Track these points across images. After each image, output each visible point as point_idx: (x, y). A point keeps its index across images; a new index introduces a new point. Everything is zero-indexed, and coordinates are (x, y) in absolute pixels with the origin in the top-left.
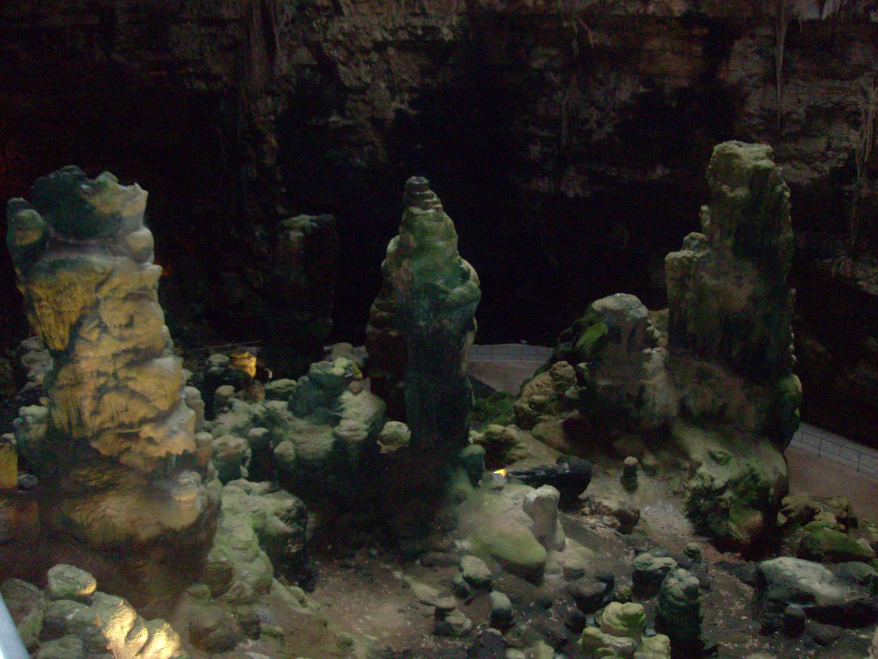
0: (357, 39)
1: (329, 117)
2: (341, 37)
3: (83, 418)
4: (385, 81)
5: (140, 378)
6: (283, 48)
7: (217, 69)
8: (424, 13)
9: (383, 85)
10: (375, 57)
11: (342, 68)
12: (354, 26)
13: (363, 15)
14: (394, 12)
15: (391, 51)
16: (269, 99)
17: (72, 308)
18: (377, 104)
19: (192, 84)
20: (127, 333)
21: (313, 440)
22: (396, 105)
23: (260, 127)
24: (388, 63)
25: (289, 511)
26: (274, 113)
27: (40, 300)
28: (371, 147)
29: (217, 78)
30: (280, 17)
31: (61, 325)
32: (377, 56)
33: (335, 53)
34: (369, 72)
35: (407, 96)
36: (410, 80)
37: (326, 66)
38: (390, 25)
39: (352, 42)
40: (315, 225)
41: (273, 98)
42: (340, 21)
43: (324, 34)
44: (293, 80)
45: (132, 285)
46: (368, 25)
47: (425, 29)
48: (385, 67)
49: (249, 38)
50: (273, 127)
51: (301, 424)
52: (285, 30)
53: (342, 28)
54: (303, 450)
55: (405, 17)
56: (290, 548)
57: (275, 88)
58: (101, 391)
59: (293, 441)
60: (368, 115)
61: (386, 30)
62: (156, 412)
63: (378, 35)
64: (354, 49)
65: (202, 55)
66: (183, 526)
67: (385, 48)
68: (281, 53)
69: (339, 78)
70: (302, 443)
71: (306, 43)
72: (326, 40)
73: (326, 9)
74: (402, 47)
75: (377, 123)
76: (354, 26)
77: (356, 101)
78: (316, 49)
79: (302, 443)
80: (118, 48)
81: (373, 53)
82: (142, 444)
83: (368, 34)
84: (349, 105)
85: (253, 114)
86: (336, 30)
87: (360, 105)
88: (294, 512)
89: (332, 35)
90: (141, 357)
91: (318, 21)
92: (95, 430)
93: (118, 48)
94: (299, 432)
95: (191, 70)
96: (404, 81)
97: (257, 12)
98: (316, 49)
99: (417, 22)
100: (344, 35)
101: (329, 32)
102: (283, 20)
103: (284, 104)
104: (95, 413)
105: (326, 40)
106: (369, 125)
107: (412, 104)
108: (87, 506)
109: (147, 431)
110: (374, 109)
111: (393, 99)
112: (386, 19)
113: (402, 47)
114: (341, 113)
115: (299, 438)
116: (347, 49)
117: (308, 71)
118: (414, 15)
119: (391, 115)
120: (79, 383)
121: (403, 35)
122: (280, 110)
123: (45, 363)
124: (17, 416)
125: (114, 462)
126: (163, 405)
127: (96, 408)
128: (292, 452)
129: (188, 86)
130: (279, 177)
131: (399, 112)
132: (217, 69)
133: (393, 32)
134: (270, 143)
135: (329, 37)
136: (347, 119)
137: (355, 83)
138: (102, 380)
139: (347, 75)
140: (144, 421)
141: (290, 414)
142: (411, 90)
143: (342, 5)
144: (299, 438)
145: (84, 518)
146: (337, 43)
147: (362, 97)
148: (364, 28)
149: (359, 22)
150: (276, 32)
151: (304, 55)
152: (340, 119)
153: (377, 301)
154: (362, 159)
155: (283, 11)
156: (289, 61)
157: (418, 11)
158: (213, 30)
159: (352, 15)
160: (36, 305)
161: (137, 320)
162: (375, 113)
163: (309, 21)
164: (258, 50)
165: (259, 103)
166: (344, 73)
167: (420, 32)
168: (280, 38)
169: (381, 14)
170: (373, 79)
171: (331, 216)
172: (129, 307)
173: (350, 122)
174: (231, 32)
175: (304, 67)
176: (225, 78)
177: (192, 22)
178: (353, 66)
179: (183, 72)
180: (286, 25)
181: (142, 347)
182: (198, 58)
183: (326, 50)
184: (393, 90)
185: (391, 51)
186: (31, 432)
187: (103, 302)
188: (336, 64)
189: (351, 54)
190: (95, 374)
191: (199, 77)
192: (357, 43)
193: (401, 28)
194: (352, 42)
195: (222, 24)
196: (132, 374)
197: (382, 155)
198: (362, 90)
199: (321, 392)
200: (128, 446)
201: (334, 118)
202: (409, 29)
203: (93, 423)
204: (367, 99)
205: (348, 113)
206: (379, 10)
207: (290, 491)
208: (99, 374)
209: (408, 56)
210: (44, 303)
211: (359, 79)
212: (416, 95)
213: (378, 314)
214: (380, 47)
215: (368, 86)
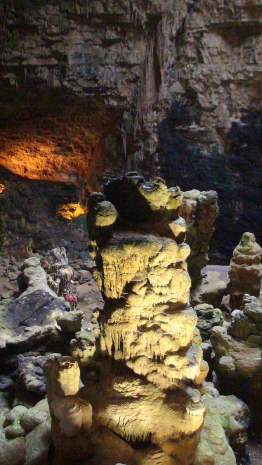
0: (212, 78)
1: (190, 125)
2: (201, 77)
3: (124, 346)
4: (226, 105)
5: (170, 323)
6: (165, 82)
7: (125, 93)
8: (255, 63)
9: (225, 107)
10: (221, 89)
11: (200, 96)
12: (210, 70)
13: (216, 63)
14: (236, 62)
15: (232, 86)
16: (155, 112)
17: (130, 273)
18: (221, 118)
19: (108, 102)
20: (164, 291)
21: (248, 358)
22: (232, 119)
23: (148, 129)
24: (229, 93)
25: (239, 412)
26: (157, 121)
27: (108, 264)
28: (214, 145)
29: (125, 98)
30: (165, 63)
31: (120, 283)
32: (223, 89)
33: (197, 86)
34: (217, 99)
35: (239, 114)
36: (243, 105)
37: (191, 94)
38: (232, 71)
39: (208, 80)
40: (205, 197)
41: (157, 113)
42: (201, 67)
43: (191, 74)
44: (170, 102)
45: (174, 260)
46: (219, 70)
47: (254, 72)
48: (228, 96)
49: (145, 75)
50: (156, 129)
51: (239, 345)
52: (168, 71)
53: (202, 71)
54: (241, 365)
55: (242, 66)
56: (240, 440)
57: (158, 106)
58: (143, 329)
59: (233, 357)
60: (214, 125)
61: (230, 73)
62: (179, 347)
63: (225, 76)
64: (209, 84)
65: (116, 84)
66: (191, 431)
67: (228, 84)
68: (164, 86)
69: (198, 102)
70: (240, 359)
71: (180, 80)
72: (192, 78)
73: (193, 59)
74: (239, 84)
75: (220, 130)
76: (210, 70)
77: (208, 116)
78: (185, 83)
79: (240, 359)
80: (67, 79)
81: (220, 87)
82: (166, 368)
83: (219, 76)
84: (203, 118)
85: (145, 121)
86: (198, 73)
87: (210, 119)
88: (243, 413)
89: (196, 75)
90: (175, 308)
91: (188, 66)
92: (132, 356)
93: (67, 79)
94: (237, 351)
95: (109, 93)
96: (239, 105)
97: (151, 60)
98: (185, 83)
99: (250, 68)
100: (204, 75)
101: (194, 73)
102: (166, 65)
103: (163, 116)
104: (134, 344)
105: (192, 78)
106: (214, 131)
107: (243, 119)
108: (125, 411)
109: (171, 360)
110: (219, 121)
111: (231, 116)
112: (230, 66)
113: (239, 84)
114: (198, 123)
115: (237, 355)
116: (205, 84)
117: (179, 97)
118: (249, 64)
119: (229, 126)
120: (127, 322)
121: (241, 77)
122: (160, 120)
123: (39, 275)
124: (74, 337)
125: (143, 380)
126: (184, 343)
127: (136, 340)
128: (232, 365)
129: (106, 103)
130: (157, 160)
131: (234, 124)
132: (124, 94)
133: (235, 74)
134: (153, 139)
135: (194, 77)
136: (201, 127)
137: (208, 105)
138: (144, 322)
139: (203, 100)
140: (170, 353)
141: (230, 337)
142: (243, 110)
143: (204, 57)
144: (237, 355)
145: (122, 419)
146: (199, 80)
147: (212, 114)
148: (216, 72)
149: (213, 67)
150: (162, 72)
151: (178, 87)
152: (197, 126)
153: (239, 247)
154: (208, 152)
155: (167, 60)
156: (168, 90)
157: (252, 62)
158: (124, 70)
159: (209, 63)
160: (105, 267)
161: (174, 283)
162: (219, 123)
163: (182, 66)
164: (150, 83)
165: (148, 115)
166: (202, 99)
167: (251, 75)
168: (164, 75)
169: (228, 63)
170: (219, 103)
171: (215, 192)
172: (171, 273)
173: (203, 129)
174: (134, 72)
175: (177, 94)
176: (128, 99)
177: (112, 65)
178: (208, 95)
179: (104, 94)
180: (169, 68)
181: (174, 301)
182: (114, 86)
183: (191, 84)
184: (232, 110)
185: (232, 86)
186: (85, 352)
187: (153, 269)
188: (196, 93)
189: (207, 87)
190: (139, 318)
191: (113, 98)
192: (211, 81)
193: (241, 72)
194: (208, 80)
195: (129, 66)
196: (166, 319)
197: (221, 151)
198: (212, 110)
199: (254, 325)
200: (155, 369)
201: (193, 126)
202: (245, 73)
203: (130, 351)
204: (215, 115)
205: (202, 123)
206: (226, 61)
207: (238, 397)
208: (142, 318)
209: (243, 90)
210: (110, 267)
211: (211, 102)
212: (245, 114)
213: (239, 256)
214: (225, 83)
215: (215, 107)
